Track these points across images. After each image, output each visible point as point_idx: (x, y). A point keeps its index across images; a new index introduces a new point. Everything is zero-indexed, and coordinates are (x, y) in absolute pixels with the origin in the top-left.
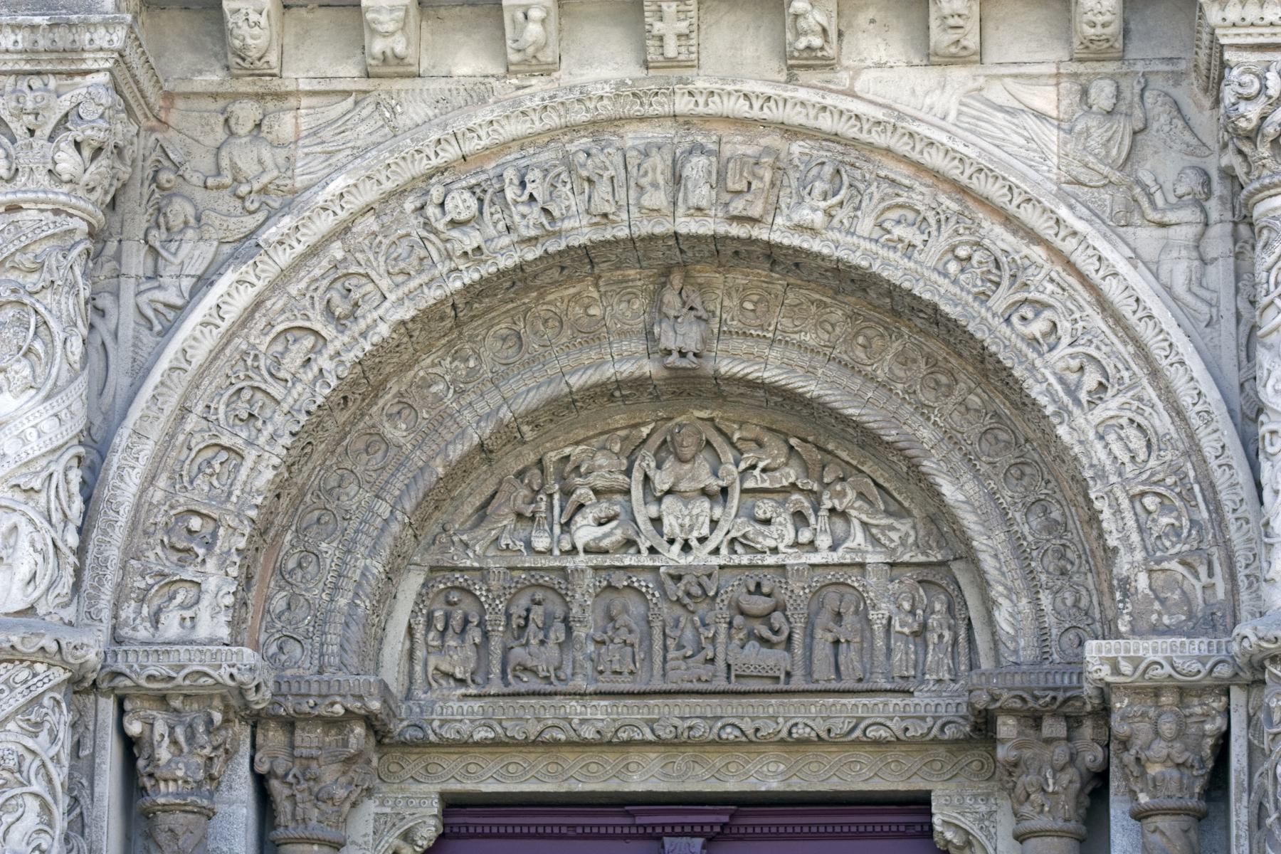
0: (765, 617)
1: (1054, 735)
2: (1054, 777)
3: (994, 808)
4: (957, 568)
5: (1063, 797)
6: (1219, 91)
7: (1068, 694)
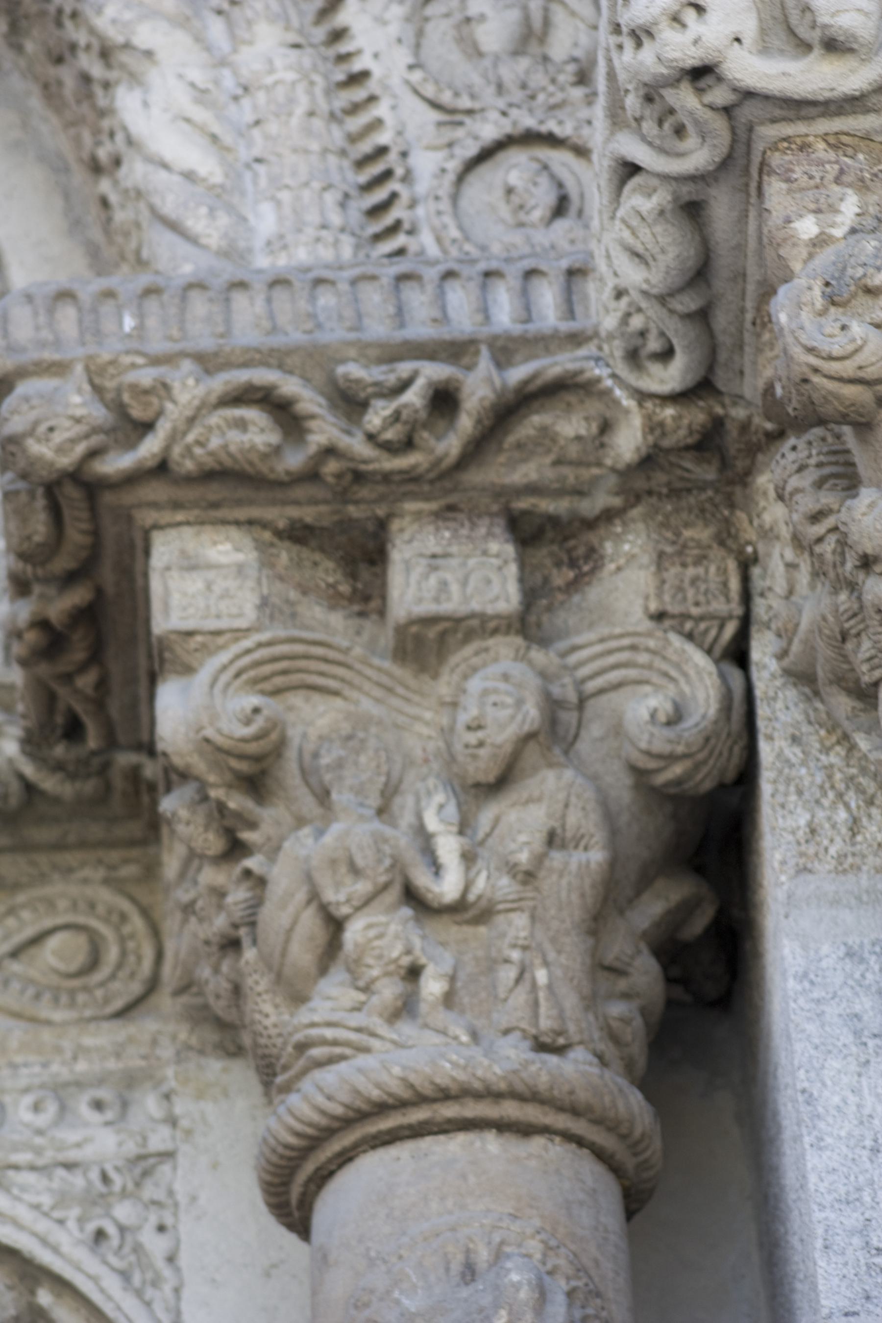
1: (452, 605)
2: (464, 827)
3: (160, 1139)
4: (89, 787)
5: (519, 922)
6: (733, 130)
7: (517, 374)
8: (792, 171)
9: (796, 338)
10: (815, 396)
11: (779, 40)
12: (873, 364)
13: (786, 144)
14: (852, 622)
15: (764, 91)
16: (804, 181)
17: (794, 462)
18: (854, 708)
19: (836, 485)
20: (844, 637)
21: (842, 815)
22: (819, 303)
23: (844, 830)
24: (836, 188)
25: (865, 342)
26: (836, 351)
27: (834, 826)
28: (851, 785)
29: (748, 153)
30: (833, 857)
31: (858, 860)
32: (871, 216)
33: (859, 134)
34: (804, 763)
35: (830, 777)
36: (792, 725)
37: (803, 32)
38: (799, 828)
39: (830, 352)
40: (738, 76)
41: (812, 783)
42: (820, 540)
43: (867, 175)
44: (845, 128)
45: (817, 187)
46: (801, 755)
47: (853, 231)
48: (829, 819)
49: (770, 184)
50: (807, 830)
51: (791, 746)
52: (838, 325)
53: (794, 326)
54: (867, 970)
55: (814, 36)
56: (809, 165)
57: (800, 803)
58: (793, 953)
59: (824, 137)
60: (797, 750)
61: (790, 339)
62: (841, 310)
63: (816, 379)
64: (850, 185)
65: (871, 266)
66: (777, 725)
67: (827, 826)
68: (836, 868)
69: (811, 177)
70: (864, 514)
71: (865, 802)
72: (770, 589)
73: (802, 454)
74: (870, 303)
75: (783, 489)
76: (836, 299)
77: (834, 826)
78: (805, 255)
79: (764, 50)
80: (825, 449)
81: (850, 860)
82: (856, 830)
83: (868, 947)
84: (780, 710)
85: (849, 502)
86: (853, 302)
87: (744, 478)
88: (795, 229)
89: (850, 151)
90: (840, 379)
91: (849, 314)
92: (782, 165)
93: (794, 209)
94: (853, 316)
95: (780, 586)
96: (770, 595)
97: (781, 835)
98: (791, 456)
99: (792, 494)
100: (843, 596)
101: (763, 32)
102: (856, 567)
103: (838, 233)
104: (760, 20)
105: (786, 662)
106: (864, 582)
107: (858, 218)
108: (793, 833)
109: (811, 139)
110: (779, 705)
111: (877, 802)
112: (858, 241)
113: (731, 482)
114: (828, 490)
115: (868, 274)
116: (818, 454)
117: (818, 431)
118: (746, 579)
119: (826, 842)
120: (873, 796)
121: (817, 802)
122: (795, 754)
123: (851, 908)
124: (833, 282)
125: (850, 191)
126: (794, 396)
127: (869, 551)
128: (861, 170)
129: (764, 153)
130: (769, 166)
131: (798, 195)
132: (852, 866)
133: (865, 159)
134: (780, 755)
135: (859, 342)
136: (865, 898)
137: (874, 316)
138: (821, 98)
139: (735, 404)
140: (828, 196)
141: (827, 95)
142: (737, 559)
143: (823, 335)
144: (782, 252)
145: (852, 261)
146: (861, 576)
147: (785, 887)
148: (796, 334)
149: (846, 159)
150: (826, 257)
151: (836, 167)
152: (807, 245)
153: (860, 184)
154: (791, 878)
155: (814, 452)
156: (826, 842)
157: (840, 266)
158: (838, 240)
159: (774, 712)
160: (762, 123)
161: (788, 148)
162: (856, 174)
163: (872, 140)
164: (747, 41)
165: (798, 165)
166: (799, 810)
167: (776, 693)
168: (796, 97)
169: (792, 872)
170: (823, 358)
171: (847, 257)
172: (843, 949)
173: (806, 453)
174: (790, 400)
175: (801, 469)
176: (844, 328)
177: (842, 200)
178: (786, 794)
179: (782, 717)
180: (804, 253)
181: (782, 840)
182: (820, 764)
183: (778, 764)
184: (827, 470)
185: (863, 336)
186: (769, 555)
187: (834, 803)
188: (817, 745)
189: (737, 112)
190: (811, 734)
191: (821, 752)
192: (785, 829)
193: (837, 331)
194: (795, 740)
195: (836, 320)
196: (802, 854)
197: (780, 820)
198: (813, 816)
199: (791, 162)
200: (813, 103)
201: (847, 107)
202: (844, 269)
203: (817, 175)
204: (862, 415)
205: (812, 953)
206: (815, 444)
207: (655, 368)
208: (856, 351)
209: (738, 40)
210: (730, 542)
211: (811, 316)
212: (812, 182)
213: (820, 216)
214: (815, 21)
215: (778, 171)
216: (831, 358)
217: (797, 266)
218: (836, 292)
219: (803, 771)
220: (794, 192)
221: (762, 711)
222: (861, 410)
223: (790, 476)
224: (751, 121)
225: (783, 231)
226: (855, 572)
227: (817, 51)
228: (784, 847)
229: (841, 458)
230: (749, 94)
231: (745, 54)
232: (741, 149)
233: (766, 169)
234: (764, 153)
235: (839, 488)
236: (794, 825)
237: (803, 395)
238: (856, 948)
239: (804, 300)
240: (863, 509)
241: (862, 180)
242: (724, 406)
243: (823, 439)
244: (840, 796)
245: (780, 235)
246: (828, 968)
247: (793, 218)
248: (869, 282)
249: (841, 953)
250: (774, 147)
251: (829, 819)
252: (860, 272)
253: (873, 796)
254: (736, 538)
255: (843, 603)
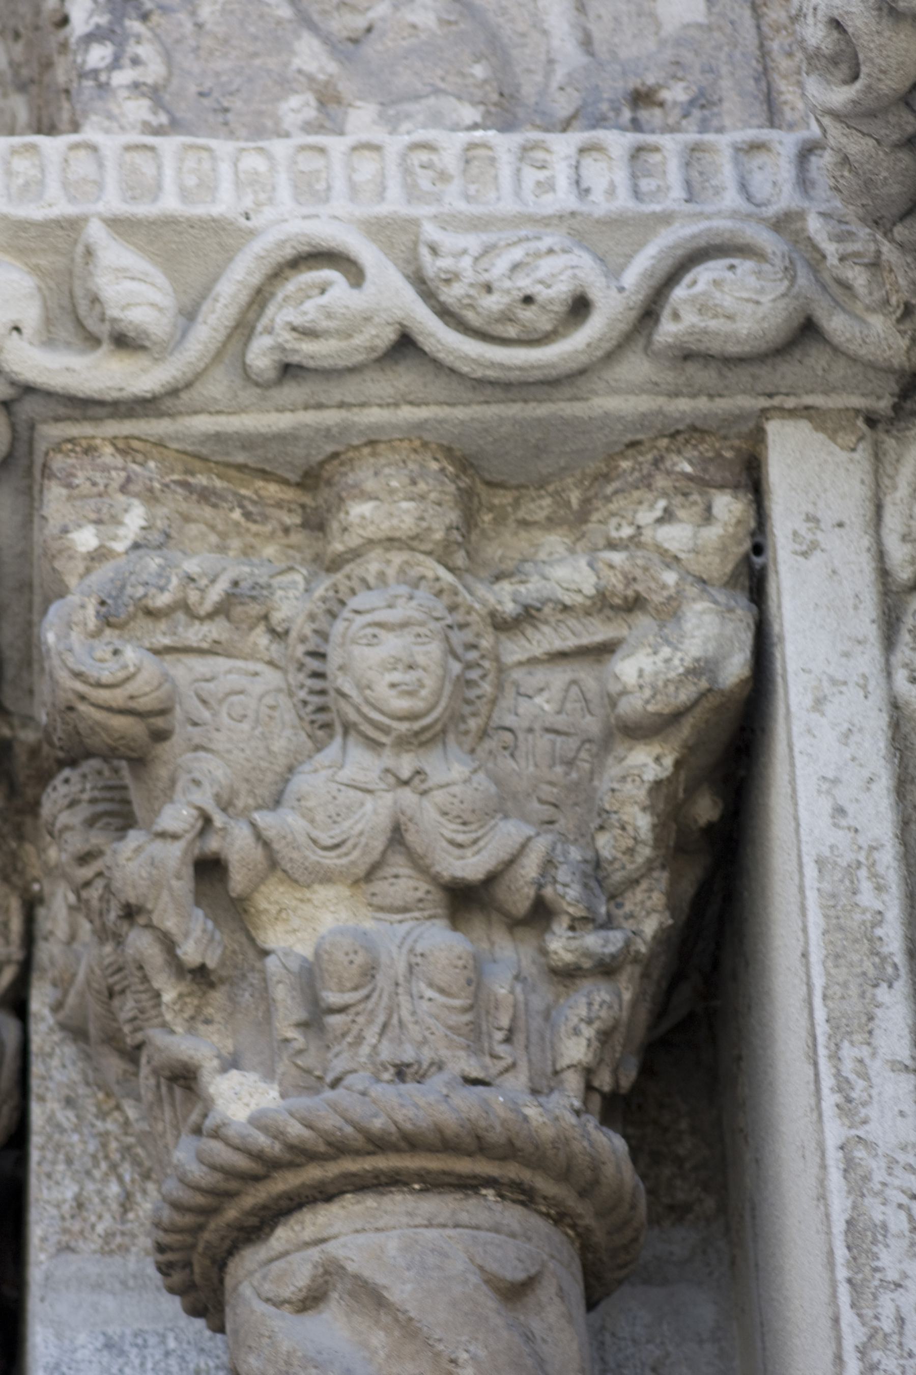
6: (13, 427)
8: (74, 476)
9: (63, 661)
10: (81, 727)
11: (65, 331)
12: (146, 694)
13: (70, 446)
14: (116, 978)
15: (45, 386)
16: (86, 488)
17: (65, 796)
18: (125, 1072)
19: (109, 824)
20: (111, 994)
21: (114, 1189)
22: (92, 623)
23: (115, 1206)
24: (121, 498)
25: (139, 670)
26: (106, 677)
27: (104, 1201)
28: (127, 1156)
29: (31, 452)
30: (100, 1236)
31: (127, 1240)
32: (159, 530)
33: (151, 439)
34: (76, 1129)
35: (104, 1145)
36: (68, 1086)
37: (92, 324)
38: (64, 1201)
39: (99, 679)
40: (16, 368)
41: (84, 1152)
42: (87, 884)
43: (157, 485)
44: (136, 432)
45: (100, 495)
46: (74, 1120)
47: (136, 546)
48: (99, 1192)
49: (49, 489)
50: (74, 1204)
51: (64, 1108)
52: (110, 649)
53: (61, 647)
54: (126, 1364)
55: (103, 330)
56: (93, 470)
57: (69, 1174)
58: (45, 1341)
59: (113, 441)
60: (71, 1114)
61: (56, 662)
62: (117, 632)
63: (83, 707)
64: (137, 495)
65: (153, 585)
66: (51, 1085)
67: (96, 1200)
68: (102, 1248)
69: (94, 484)
70: (129, 859)
71: (140, 1175)
72: (51, 933)
73: (75, 787)
74: (151, 626)
75: (53, 825)
76: (111, 619)
77: (104, 1201)
78: (81, 568)
79: (49, 342)
80: (101, 784)
81: (119, 1240)
82: (128, 1206)
83: (129, 1338)
84: (56, 1068)
85: (115, 845)
86: (132, 624)
87: (34, 807)
88: (72, 540)
89: (140, 458)
90: (110, 709)
91: (127, 637)
92: (64, 469)
93: (73, 518)
94: (128, 641)
95: (61, 930)
96: (52, 939)
97: (45, 1209)
98: (63, 789)
99: (61, 831)
100: (108, 948)
101: (48, 321)
102: (120, 917)
103: (119, 547)
104: (46, 308)
105: (61, 1015)
106: (127, 935)
107: (144, 532)
108: (58, 1206)
109: (98, 442)
110: (55, 1062)
111: (154, 1176)
112: (141, 558)
113: (20, 812)
114: (101, 829)
115: (150, 594)
116: (93, 789)
117: (95, 763)
118: (29, 920)
119: (93, 1219)
120: (150, 1170)
121: (88, 1173)
122: (68, 1119)
123: (114, 1294)
124: (110, 601)
125: (136, 502)
126: (59, 724)
127: (133, 901)
128: (151, 479)
129: (47, 454)
130: (50, 469)
131: (78, 503)
132: (120, 1247)
133: (157, 467)
134: (51, 1119)
135: (132, 669)
136: (131, 1283)
137: (154, 640)
138: (108, 398)
139: (24, 726)
140: (111, 506)
141: (115, 395)
142: (21, 897)
143: (94, 659)
144: (57, 565)
145: (133, 579)
146: (125, 927)
147: (44, 1267)
148: (64, 657)
149: (136, 467)
150: (104, 573)
151: (123, 474)
152: (84, 559)
153: (149, 494)
154: (51, 1257)
155: (88, 786)
156: (93, 1219)
157: (118, 583)
158: (119, 555)
159: (48, 1069)
160: (45, 421)
161: (72, 451)
162: (145, 484)
163: (166, 447)
164: (27, 331)
165: (82, 469)
166: (67, 1181)
167: (53, 1049)
168: (81, 395)
169: (52, 1250)
170: (91, 685)
171: (127, 574)
172: (101, 1339)
173: (79, 787)
174: (55, 729)
175: (73, 804)
176: (116, 652)
177: (126, 511)
178: (54, 1163)
179: (58, 1076)
180: (81, 567)
181: (46, 1214)
182: (95, 1131)
183: (48, 1129)
184: (101, 807)
185: (137, 662)
186: (53, 894)
187: (106, 1174)
188: (93, 1110)
189: (17, 408)
190: (87, 1096)
191: (97, 1117)
192: (48, 1202)
193: (108, 655)
194: (69, 1102)
195: (109, 643)
196: (65, 1231)
197: (45, 1192)
198: (82, 1189)
199: (73, 466)
200: (101, 403)
201: (138, 409)
202: (123, 588)
203: (101, 482)
204: (132, 750)
205: (67, 1342)
206: (90, 777)
207: (430, 574)
208: (128, 679)
209: (17, 329)
210: (15, 879)
211: (82, 637)
212: (95, 490)
213: (101, 527)
214: (103, 314)
215: (59, 475)
216: (99, 685)
217: (72, 581)
218: (112, 611)
219: (75, 1138)
220: (75, 498)
221: (37, 1068)
222: (132, 744)
223: (60, 811)
224: (32, 419)
225: (60, 542)
226: (119, 923)
227: (106, 347)
228: (46, 1222)
229: (117, 795)
230: (29, 390)
231: (25, 345)
232: (22, 449)
233: (47, 471)
234: (47, 454)
235: (112, 828)
236: (60, 1197)
237: (68, 724)
238: (116, 1338)
239: (75, 618)
240: (128, 854)
241: (151, 490)
242: (12, 727)
243: (100, 773)
244: (114, 1167)
245: (55, 546)
246: (83, 1361)
247: (71, 527)
248: (150, 603)
249: (99, 1344)
250: (57, 448)
251: (99, 1192)
252: (140, 591)
253: (150, 1170)
254: (22, 873)
255: (108, 956)
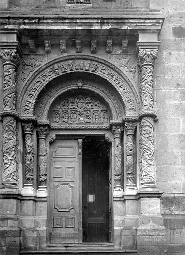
0: (88, 116)
